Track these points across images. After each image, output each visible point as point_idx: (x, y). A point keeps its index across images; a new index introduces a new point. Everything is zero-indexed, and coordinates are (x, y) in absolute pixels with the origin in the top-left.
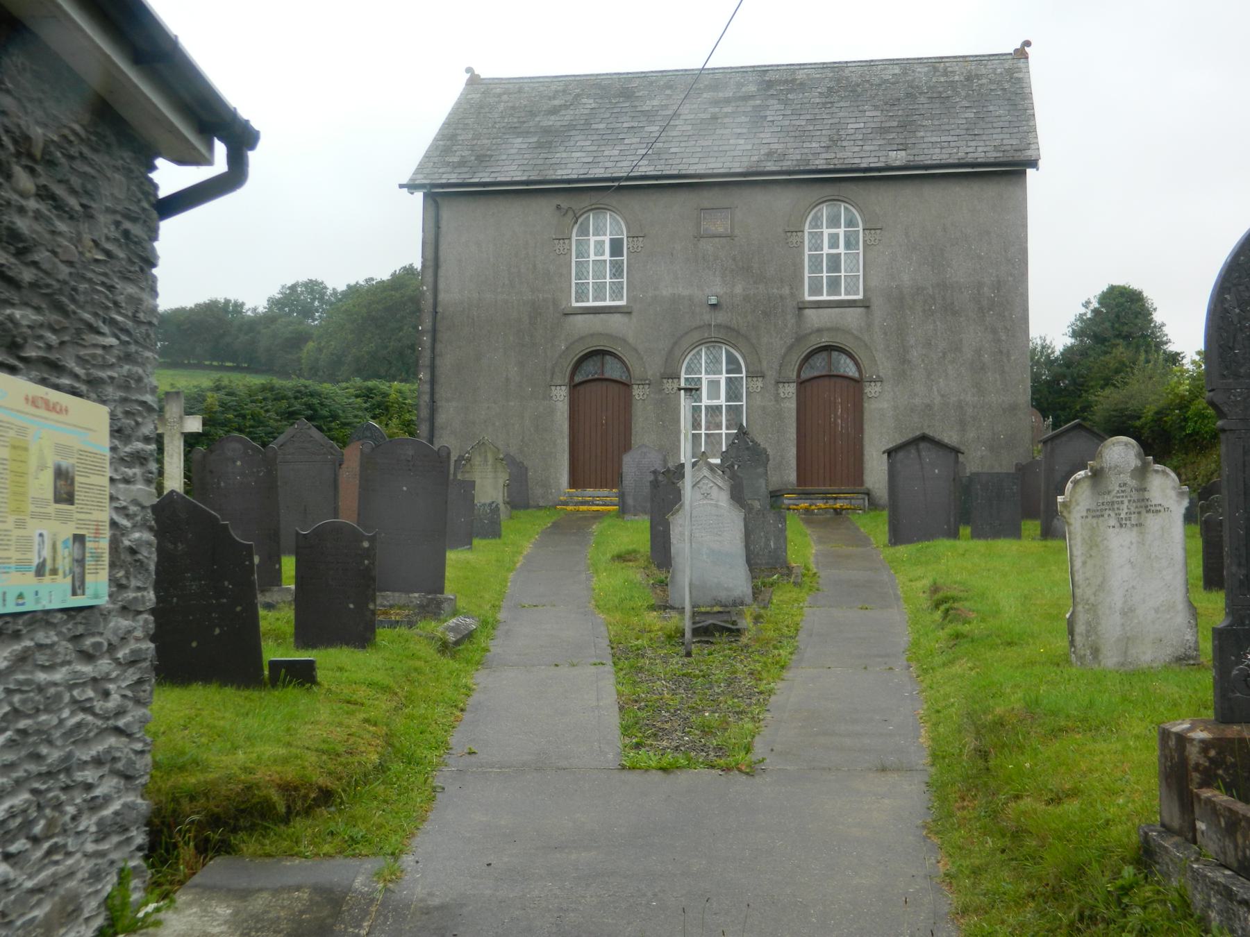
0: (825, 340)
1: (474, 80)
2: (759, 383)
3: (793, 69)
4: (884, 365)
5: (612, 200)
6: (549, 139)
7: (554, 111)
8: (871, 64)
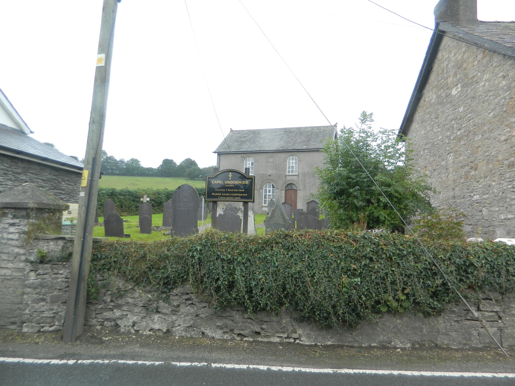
0: (290, 182)
1: (232, 131)
2: (278, 190)
3: (291, 128)
4: (301, 187)
5: (252, 155)
6: (243, 143)
7: (245, 137)
8: (306, 127)
